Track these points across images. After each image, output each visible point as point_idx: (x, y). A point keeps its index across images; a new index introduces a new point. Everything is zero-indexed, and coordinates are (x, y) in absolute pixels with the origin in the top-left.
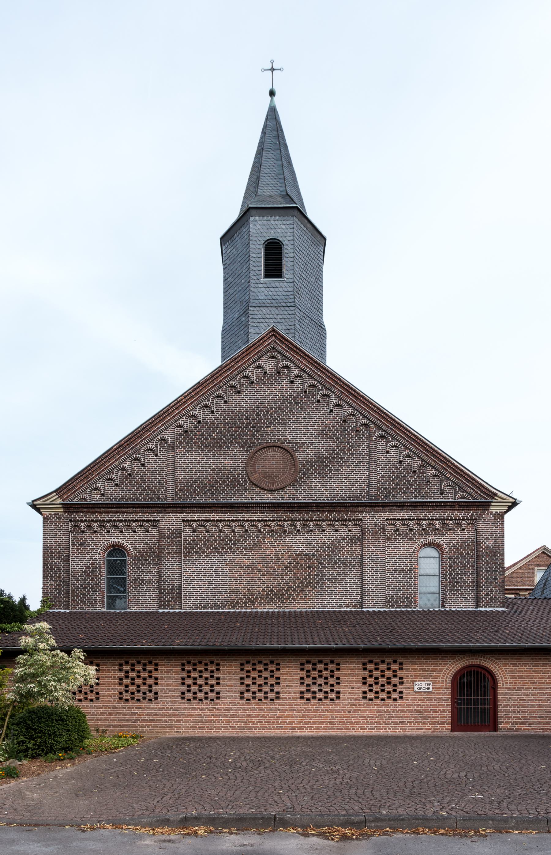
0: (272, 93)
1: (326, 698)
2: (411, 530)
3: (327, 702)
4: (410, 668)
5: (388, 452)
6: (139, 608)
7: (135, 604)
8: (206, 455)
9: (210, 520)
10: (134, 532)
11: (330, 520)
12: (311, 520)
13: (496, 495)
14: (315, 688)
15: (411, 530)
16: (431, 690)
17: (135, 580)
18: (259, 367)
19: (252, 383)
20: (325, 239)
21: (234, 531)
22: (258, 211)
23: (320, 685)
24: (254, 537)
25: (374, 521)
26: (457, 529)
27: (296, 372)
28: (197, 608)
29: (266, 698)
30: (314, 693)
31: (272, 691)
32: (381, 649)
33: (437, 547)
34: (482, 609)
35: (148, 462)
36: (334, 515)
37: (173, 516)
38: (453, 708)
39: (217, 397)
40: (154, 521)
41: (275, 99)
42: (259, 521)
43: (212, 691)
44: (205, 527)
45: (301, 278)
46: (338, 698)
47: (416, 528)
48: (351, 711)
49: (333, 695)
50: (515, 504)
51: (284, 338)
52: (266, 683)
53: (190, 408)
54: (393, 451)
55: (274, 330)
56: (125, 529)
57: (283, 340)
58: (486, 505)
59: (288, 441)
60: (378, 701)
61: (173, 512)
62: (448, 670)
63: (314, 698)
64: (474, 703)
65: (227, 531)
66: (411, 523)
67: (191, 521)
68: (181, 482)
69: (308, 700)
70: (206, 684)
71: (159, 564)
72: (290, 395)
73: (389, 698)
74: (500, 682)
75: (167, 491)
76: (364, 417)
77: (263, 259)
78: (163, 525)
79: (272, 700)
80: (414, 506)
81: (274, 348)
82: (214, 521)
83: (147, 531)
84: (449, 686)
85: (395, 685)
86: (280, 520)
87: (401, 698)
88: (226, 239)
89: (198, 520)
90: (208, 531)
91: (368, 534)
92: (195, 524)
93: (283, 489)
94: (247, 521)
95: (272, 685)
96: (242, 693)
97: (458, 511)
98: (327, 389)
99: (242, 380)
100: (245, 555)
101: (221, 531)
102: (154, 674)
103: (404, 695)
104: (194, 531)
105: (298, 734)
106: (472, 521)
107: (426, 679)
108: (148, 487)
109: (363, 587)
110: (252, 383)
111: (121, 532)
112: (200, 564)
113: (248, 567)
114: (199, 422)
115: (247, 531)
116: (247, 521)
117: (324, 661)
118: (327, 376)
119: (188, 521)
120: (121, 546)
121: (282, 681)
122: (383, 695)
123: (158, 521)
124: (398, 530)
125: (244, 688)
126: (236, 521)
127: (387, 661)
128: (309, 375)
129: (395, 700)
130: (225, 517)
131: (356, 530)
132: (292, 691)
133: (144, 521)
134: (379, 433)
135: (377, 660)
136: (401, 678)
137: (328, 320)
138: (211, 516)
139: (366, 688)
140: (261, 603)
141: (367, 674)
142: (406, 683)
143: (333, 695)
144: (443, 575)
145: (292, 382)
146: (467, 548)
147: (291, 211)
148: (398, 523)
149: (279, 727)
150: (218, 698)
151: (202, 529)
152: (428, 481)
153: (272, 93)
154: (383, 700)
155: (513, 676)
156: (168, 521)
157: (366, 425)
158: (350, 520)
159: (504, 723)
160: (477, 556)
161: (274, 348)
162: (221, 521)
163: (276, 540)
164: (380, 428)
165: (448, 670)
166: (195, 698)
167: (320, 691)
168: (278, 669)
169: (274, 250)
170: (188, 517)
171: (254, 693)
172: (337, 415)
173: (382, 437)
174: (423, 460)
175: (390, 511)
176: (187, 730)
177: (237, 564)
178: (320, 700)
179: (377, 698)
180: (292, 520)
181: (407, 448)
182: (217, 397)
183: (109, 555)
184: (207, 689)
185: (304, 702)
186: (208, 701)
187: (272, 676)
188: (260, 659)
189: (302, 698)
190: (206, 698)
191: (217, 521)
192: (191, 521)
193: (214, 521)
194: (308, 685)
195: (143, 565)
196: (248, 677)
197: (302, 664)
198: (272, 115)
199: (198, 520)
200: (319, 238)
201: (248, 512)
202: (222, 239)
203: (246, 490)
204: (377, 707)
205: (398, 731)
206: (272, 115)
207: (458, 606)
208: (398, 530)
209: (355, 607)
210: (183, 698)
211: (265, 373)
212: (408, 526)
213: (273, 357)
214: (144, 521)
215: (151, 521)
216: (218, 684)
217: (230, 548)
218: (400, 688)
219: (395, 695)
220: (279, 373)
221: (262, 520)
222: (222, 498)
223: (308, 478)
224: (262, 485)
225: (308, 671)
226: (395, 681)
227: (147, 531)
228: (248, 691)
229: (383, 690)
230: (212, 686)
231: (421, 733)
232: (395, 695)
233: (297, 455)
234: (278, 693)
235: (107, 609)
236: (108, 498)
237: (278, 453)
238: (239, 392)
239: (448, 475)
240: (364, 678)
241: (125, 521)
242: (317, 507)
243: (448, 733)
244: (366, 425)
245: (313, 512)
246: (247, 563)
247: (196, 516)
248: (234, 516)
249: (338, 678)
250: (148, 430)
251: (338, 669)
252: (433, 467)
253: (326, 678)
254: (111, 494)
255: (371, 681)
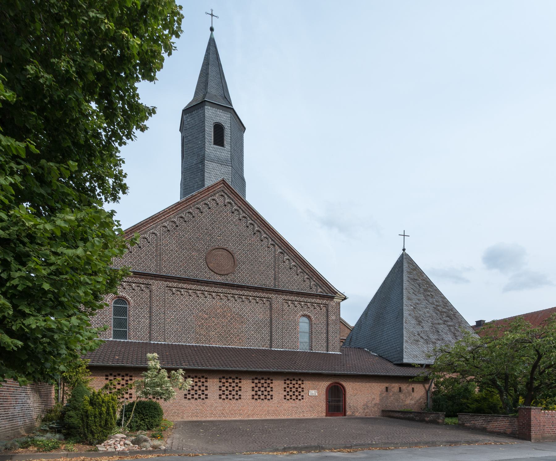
0: (212, 29)
1: (266, 398)
2: (296, 307)
3: (266, 401)
4: (307, 384)
5: (284, 262)
6: (136, 339)
7: (134, 337)
8: (181, 247)
9: (184, 288)
10: (134, 289)
11: (254, 296)
12: (244, 295)
13: (337, 293)
14: (260, 393)
15: (296, 307)
16: (317, 395)
17: (134, 321)
18: (214, 200)
19: (210, 208)
20: (245, 129)
21: (198, 296)
22: (210, 104)
23: (262, 392)
24: (211, 302)
25: (277, 300)
26: (318, 309)
27: (235, 207)
28: (175, 341)
29: (234, 398)
30: (259, 396)
31: (237, 394)
32: (291, 371)
33: (309, 317)
34: (330, 353)
35: (144, 246)
36: (256, 294)
37: (161, 283)
38: (326, 404)
39: (188, 213)
40: (148, 284)
41: (214, 33)
42: (214, 292)
43: (203, 394)
44: (181, 292)
45: (234, 150)
46: (272, 398)
47: (299, 306)
48: (278, 405)
49: (269, 397)
50: (345, 299)
51: (229, 186)
52: (233, 390)
53: (172, 216)
54: (287, 262)
55: (223, 180)
56: (127, 287)
57: (228, 187)
58: (332, 298)
59: (231, 247)
60: (292, 400)
61: (160, 280)
62: (324, 385)
63: (259, 398)
64: (336, 403)
65: (194, 296)
66: (296, 303)
67: (172, 287)
68: (165, 262)
69: (256, 399)
70: (200, 389)
71: (150, 312)
72: (232, 220)
73: (297, 399)
74: (347, 391)
75: (156, 266)
76: (272, 240)
77: (213, 133)
78: (154, 288)
79: (237, 399)
80: (298, 294)
81: (223, 191)
82: (186, 289)
83: (143, 290)
84: (325, 393)
85: (300, 392)
86: (226, 293)
87: (303, 399)
88: (186, 111)
89: (177, 287)
90: (182, 295)
91: (274, 306)
92: (174, 289)
93: (227, 274)
94: (207, 291)
95: (237, 391)
96: (220, 395)
97: (319, 299)
98: (252, 220)
99: (204, 206)
100: (205, 311)
101: (190, 296)
102: (205, 384)
103: (304, 397)
104: (174, 294)
105: (251, 418)
106: (326, 305)
107: (314, 389)
108: (143, 262)
109: (271, 336)
110: (210, 208)
111: (124, 288)
112: (177, 314)
113: (207, 319)
114: (177, 226)
115: (206, 297)
116: (207, 291)
117: (226, 377)
118: (253, 214)
119: (170, 287)
120: (124, 298)
121: (242, 389)
122: (294, 397)
123: (150, 285)
124: (289, 306)
125: (221, 392)
126: (200, 290)
127: (296, 379)
128: (242, 211)
129: (300, 400)
130: (194, 287)
131: (267, 304)
132: (248, 394)
133: (141, 283)
134: (280, 250)
135: (266, 377)
136: (303, 388)
137: (246, 176)
138: (185, 286)
139: (285, 393)
140: (214, 341)
141: (286, 386)
142: (305, 391)
143: (269, 397)
144: (311, 333)
145: (233, 213)
146: (323, 319)
147: (230, 110)
148: (289, 302)
149: (241, 415)
150: (207, 398)
151: (179, 293)
152: (304, 281)
153: (212, 29)
154: (294, 400)
155: (352, 388)
156: (156, 285)
157: (273, 245)
158: (265, 298)
159: (348, 413)
160: (328, 325)
161: (223, 191)
162: (191, 289)
163: (223, 304)
164: (280, 248)
165: (324, 385)
166: (193, 398)
167: (262, 394)
168: (240, 382)
169: (219, 129)
170: (170, 284)
171: (227, 395)
172: (258, 236)
173: (281, 253)
174: (302, 269)
175: (286, 295)
176: (188, 417)
177: (200, 316)
178: (262, 399)
179: (291, 399)
180: (233, 294)
181: (294, 261)
182: (188, 213)
183: (115, 303)
184: (200, 392)
185: (254, 400)
186: (201, 400)
187: (237, 386)
188: (111, 372)
189: (253, 398)
190: (200, 398)
191: (188, 289)
192: (172, 287)
193: (186, 289)
194: (256, 391)
195: (139, 312)
196: (224, 386)
197: (285, 380)
198: (212, 43)
199: (177, 287)
200: (242, 128)
201: (207, 286)
202: (183, 111)
203: (206, 272)
204: (291, 404)
205: (301, 416)
206: (212, 43)
207: (319, 350)
208: (289, 306)
209: (267, 347)
210: (186, 398)
211: (217, 204)
212: (294, 304)
213: (222, 195)
214: (141, 283)
215: (145, 284)
216: (206, 389)
217: (196, 306)
218: (302, 394)
219: (300, 397)
220: (225, 205)
221: (216, 292)
222: (191, 274)
223: (242, 270)
224: (215, 271)
225: (256, 384)
226: (300, 390)
227: (143, 290)
228: (224, 394)
229: (294, 395)
230: (203, 391)
231: (311, 417)
232: (300, 397)
233: (235, 256)
234: (240, 395)
235: (114, 338)
236: (115, 266)
237: (225, 253)
238: (202, 213)
239: (314, 279)
240: (285, 388)
241: (128, 282)
242: (247, 288)
243: (324, 417)
244: (273, 245)
245: (245, 290)
246: (206, 316)
247: (175, 285)
248: (199, 287)
249: (272, 388)
250: (145, 226)
251: (272, 383)
252: (307, 274)
253: (266, 388)
254: (117, 263)
255: (288, 390)
